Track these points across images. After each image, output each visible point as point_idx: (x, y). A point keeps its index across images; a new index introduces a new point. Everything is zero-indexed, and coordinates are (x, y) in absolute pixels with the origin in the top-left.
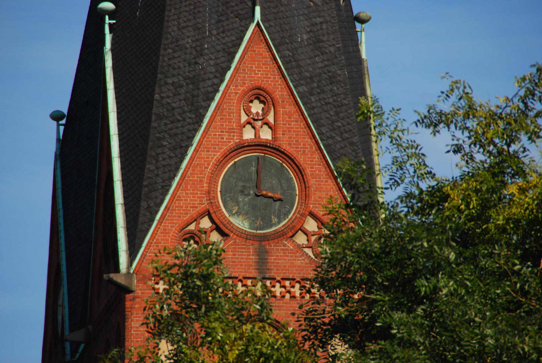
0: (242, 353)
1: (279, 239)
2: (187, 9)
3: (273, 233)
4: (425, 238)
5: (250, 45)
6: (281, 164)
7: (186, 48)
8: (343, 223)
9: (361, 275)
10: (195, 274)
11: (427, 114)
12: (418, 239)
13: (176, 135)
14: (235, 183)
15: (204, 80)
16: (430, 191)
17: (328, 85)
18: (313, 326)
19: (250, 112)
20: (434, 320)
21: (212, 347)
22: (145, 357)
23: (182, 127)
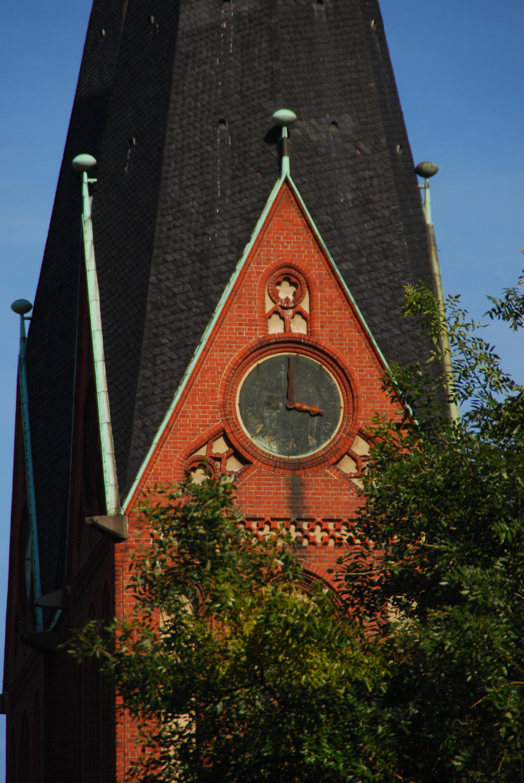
0: (261, 624)
1: (319, 467)
2: (192, 162)
3: (311, 459)
4: (504, 467)
5: (276, 208)
6: (320, 366)
7: (191, 214)
8: (394, 449)
9: (420, 518)
10: (197, 518)
11: (505, 301)
12: (495, 468)
13: (179, 329)
14: (259, 392)
15: (215, 257)
16: (509, 405)
17: (381, 260)
18: (358, 587)
19: (278, 298)
20: (520, 576)
21: (221, 615)
22: (132, 630)
23: (187, 318)
